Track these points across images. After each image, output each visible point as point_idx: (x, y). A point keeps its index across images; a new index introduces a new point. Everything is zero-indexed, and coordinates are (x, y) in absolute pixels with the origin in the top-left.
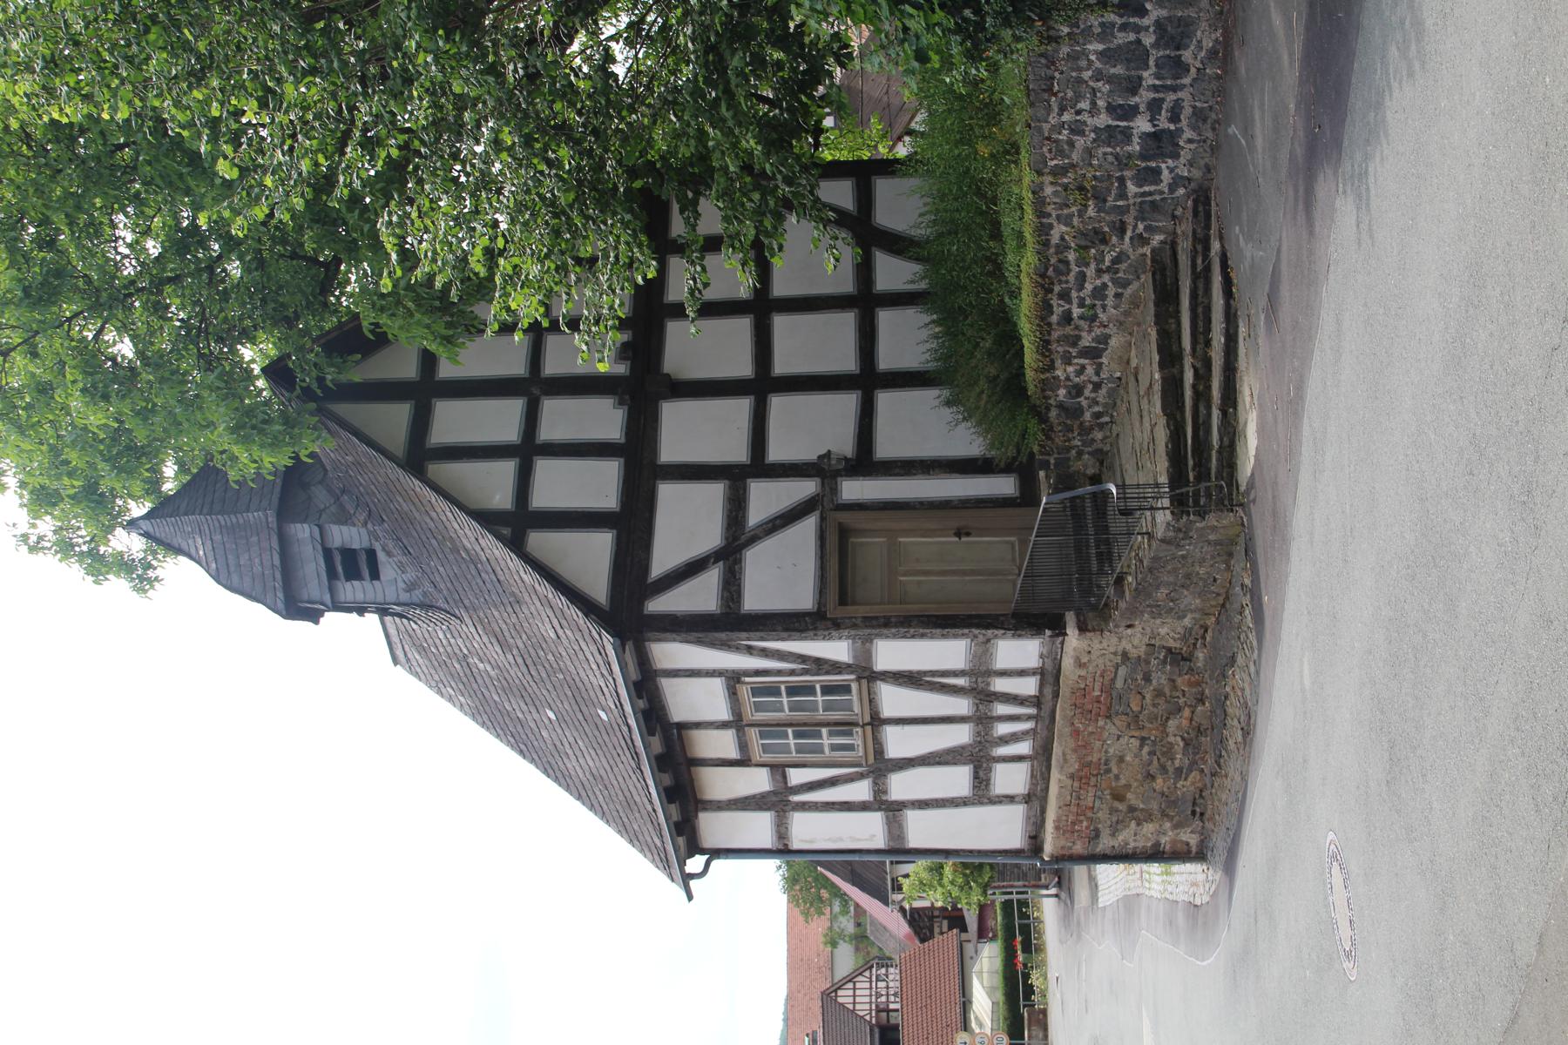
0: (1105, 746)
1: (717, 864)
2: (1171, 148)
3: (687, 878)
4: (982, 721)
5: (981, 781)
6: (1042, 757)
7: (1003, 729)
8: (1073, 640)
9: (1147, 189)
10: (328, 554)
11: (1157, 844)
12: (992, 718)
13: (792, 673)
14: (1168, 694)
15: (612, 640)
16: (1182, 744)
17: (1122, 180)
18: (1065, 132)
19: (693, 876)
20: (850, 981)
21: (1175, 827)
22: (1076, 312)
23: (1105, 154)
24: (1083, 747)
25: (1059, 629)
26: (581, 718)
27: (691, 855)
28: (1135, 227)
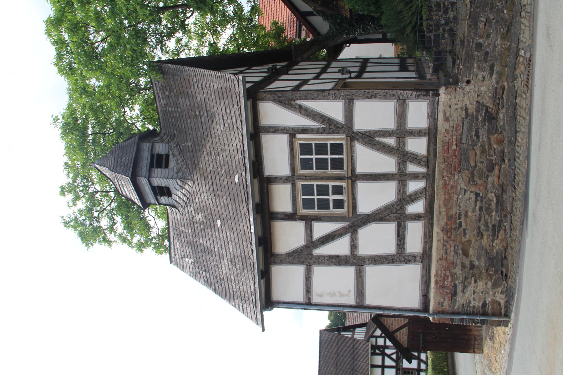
12: (406, 175)
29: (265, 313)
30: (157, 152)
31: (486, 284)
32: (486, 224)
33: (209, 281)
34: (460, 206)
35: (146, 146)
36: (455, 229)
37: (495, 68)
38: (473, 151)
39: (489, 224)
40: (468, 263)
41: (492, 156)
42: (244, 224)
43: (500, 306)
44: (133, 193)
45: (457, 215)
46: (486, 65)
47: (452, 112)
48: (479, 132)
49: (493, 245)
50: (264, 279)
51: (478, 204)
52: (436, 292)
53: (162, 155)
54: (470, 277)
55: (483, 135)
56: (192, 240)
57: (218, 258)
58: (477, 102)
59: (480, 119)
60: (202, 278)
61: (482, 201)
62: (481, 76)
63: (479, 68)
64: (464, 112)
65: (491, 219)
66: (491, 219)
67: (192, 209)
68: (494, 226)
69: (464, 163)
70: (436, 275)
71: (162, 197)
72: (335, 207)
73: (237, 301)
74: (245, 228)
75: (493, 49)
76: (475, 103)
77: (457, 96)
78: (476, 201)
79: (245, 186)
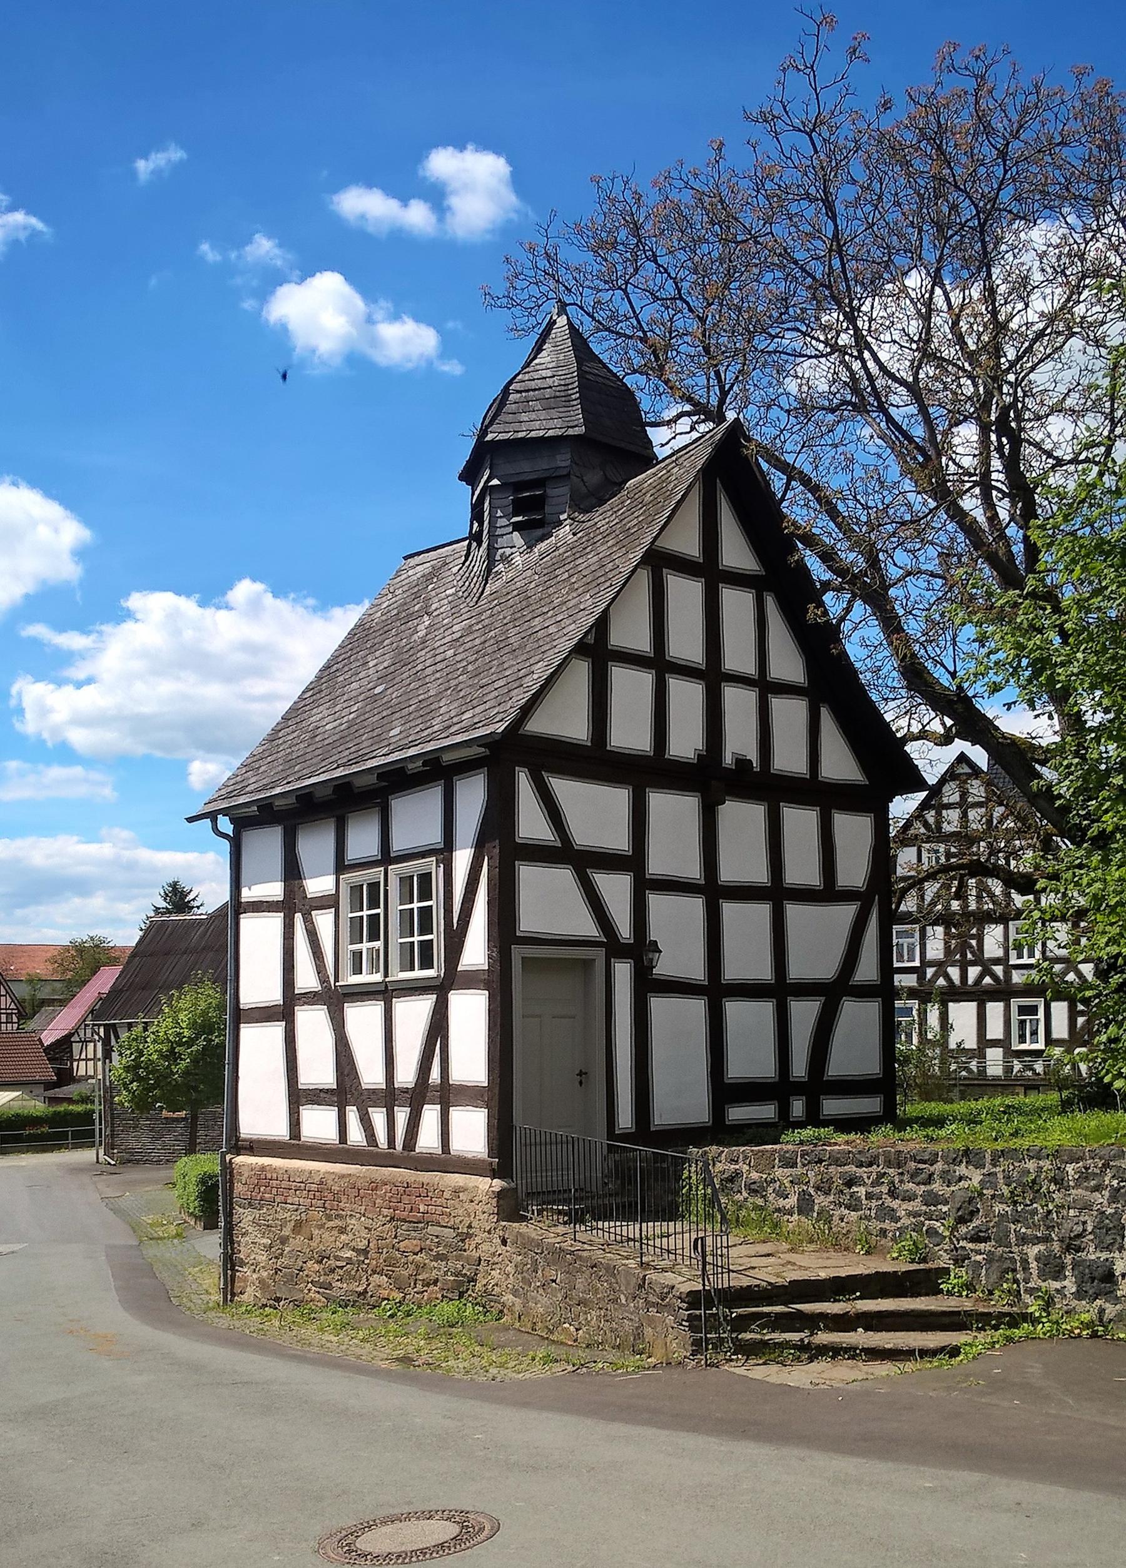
0: (358, 1215)
1: (226, 845)
2: (1091, 1292)
3: (212, 816)
4: (389, 1096)
5: (317, 1097)
6: (340, 1152)
7: (378, 1117)
8: (486, 1185)
9: (1034, 1265)
10: (539, 483)
11: (242, 1264)
13: (448, 910)
14: (420, 1277)
15: (499, 731)
16: (360, 1289)
17: (1046, 1239)
18: (1115, 1183)
19: (214, 821)
20: (7, 992)
21: (261, 1281)
22: (861, 1191)
23: (1085, 1223)
24: (357, 1191)
25: (501, 1171)
26: (385, 713)
27: (232, 821)
28: (979, 1252)
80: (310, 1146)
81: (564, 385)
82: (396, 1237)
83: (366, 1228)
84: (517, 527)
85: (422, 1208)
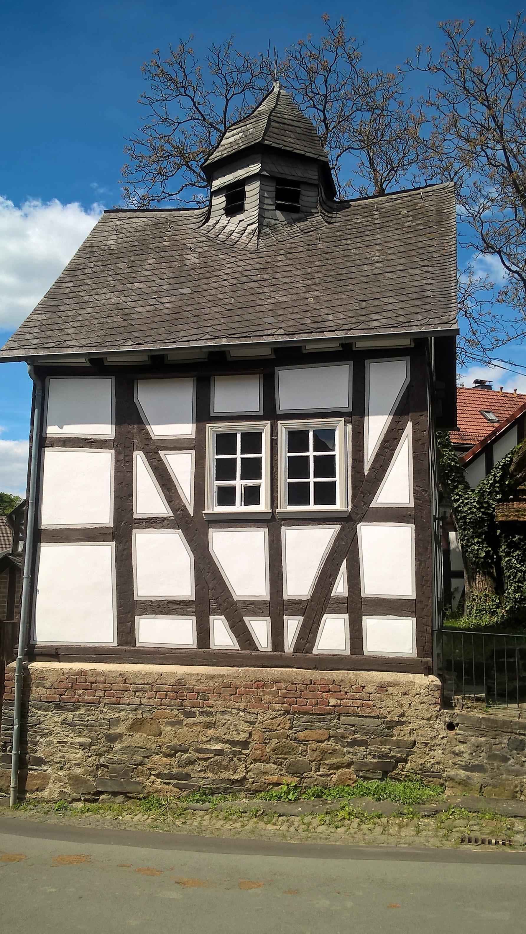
29: (25, 367)
30: (303, 192)
31: (78, 765)
32: (191, 762)
33: (79, 273)
34: (223, 713)
35: (313, 175)
36: (182, 706)
37: (476, 774)
38: (326, 737)
39: (191, 767)
40: (119, 731)
41: (318, 769)
42: (190, 331)
43: (37, 790)
44: (231, 149)
45: (208, 709)
46: (483, 759)
47: (396, 698)
48: (359, 746)
49: (151, 775)
50: (88, 364)
51: (227, 748)
52: (63, 673)
53: (298, 202)
54: (93, 734)
55: (355, 754)
56: (151, 246)
57: (120, 288)
58: (415, 743)
59: (385, 749)
60: (83, 261)
61: (234, 754)
62: (462, 749)
63: (477, 747)
64: (396, 719)
65: (201, 771)
66: (201, 771)
67: (207, 248)
68: (188, 776)
69: (303, 719)
70: (95, 673)
71: (224, 198)
72: (221, 489)
73: (44, 317)
74: (182, 334)
75: (513, 771)
76: (412, 738)
77: (425, 706)
78: (234, 743)
79: (258, 333)
80: (152, 652)
81: (309, 129)
82: (291, 728)
83: (246, 722)
84: (279, 207)
85: (332, 702)
